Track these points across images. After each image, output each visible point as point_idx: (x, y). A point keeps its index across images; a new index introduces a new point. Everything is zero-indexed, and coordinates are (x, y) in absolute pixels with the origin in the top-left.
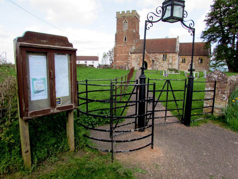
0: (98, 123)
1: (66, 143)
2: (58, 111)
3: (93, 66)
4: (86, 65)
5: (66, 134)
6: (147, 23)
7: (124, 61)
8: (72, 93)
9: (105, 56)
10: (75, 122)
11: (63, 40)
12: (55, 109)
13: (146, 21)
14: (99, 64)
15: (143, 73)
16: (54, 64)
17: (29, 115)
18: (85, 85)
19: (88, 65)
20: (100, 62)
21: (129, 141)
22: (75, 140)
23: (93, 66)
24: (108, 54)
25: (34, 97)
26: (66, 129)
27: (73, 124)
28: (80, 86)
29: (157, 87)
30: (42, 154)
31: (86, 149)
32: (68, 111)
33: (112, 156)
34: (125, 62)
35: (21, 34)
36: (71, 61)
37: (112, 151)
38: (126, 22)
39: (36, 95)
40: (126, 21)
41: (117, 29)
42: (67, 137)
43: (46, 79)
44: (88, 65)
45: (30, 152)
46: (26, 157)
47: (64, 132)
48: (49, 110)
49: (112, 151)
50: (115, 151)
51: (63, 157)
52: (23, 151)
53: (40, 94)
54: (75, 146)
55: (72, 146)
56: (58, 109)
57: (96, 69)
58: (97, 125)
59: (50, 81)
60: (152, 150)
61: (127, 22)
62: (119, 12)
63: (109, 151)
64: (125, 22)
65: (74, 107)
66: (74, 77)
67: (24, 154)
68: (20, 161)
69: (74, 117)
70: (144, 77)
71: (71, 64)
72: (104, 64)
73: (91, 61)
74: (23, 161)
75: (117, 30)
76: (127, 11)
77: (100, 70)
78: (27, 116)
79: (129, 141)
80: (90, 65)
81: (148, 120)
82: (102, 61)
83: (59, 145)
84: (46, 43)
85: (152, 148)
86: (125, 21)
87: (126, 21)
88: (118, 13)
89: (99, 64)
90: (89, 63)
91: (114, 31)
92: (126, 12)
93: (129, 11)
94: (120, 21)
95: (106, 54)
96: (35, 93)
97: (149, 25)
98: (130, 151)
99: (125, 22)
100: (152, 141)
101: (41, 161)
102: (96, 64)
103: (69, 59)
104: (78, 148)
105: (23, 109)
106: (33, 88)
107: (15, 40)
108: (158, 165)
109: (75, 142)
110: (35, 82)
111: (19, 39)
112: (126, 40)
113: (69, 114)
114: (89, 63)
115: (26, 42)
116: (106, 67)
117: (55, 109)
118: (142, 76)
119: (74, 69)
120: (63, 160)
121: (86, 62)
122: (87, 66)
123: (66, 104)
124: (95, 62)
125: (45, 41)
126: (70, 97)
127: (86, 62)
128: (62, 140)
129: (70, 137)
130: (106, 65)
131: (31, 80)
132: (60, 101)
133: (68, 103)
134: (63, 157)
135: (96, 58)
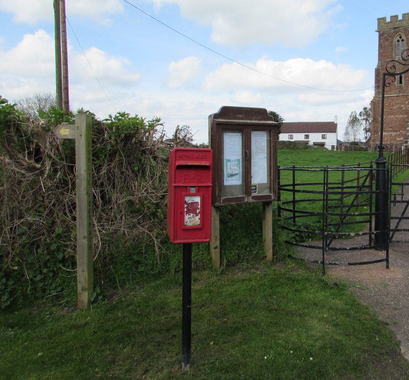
0: (311, 237)
1: (262, 248)
2: (253, 201)
3: (322, 145)
4: (307, 143)
5: (261, 236)
6: (386, 77)
7: (397, 132)
8: (271, 180)
9: (354, 121)
10: (274, 222)
11: (261, 113)
12: (250, 198)
13: (385, 75)
14: (337, 140)
15: (381, 155)
16: (251, 142)
17: (222, 202)
18: (292, 171)
19: (311, 143)
20: (342, 134)
21: (347, 250)
22: (274, 246)
23: (322, 145)
24: (360, 115)
25: (228, 182)
26: (262, 231)
27: (271, 225)
28: (283, 173)
29: (264, 144)
30: (232, 255)
31: (288, 260)
32: (266, 203)
33: (324, 269)
34: (399, 136)
35: (216, 110)
36: (270, 137)
37: (323, 263)
38: (400, 40)
39: (229, 179)
40: (400, 37)
41: (379, 58)
42: (264, 240)
43: (241, 160)
44: (311, 143)
45: (219, 248)
46: (215, 254)
47: (259, 234)
48: (243, 198)
49: (323, 263)
50: (327, 262)
51: (257, 266)
52: (213, 245)
53: (234, 178)
54: (273, 255)
55: (269, 254)
56: (254, 198)
57: (330, 151)
58: (310, 240)
59: (245, 162)
60: (387, 270)
61: (403, 40)
62: (384, 19)
63: (320, 262)
64: (398, 41)
65: (273, 198)
66: (274, 159)
67: (212, 250)
68: (209, 258)
69: (273, 216)
70: (382, 161)
71: (270, 140)
72: (352, 139)
73: (320, 135)
74: (211, 258)
75: (379, 60)
76: (391, 17)
77: (338, 155)
78: (220, 202)
79: (347, 250)
80: (315, 144)
81: (394, 233)
82: (347, 133)
83: (253, 249)
84: (242, 119)
85: (388, 267)
86: (398, 38)
87: (400, 37)
88: (381, 21)
89: (337, 140)
90: (315, 138)
91: (372, 61)
92: (400, 18)
93: (396, 17)
94: (387, 40)
95: (358, 117)
96: (228, 177)
97: (389, 79)
98: (350, 264)
99: (398, 41)
100: (387, 256)
101: (231, 265)
102: (330, 141)
103: (268, 136)
104: (277, 258)
105: (215, 193)
106: (227, 171)
107: (210, 116)
108: (388, 285)
109: (273, 248)
110: (229, 164)
111: (216, 116)
112: (401, 82)
113: (267, 208)
114: (315, 138)
115: (224, 119)
116: (354, 146)
117: (250, 198)
118: (380, 160)
119: (275, 148)
120: (257, 269)
121: (307, 137)
122: (310, 147)
123: (264, 192)
124: (329, 135)
125: (241, 116)
126: (268, 185)
127: (323, 137)
128: (256, 243)
129: (267, 239)
130: (355, 144)
131: (225, 161)
132: (256, 189)
133: (266, 193)
134: (257, 266)
135: (331, 127)
